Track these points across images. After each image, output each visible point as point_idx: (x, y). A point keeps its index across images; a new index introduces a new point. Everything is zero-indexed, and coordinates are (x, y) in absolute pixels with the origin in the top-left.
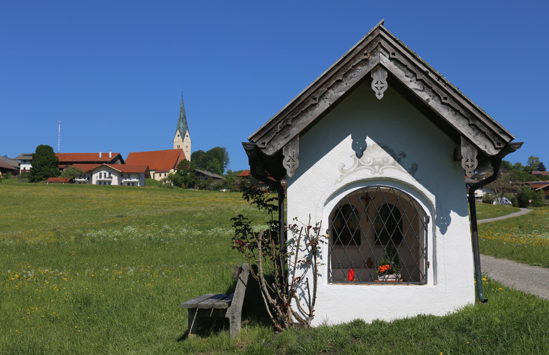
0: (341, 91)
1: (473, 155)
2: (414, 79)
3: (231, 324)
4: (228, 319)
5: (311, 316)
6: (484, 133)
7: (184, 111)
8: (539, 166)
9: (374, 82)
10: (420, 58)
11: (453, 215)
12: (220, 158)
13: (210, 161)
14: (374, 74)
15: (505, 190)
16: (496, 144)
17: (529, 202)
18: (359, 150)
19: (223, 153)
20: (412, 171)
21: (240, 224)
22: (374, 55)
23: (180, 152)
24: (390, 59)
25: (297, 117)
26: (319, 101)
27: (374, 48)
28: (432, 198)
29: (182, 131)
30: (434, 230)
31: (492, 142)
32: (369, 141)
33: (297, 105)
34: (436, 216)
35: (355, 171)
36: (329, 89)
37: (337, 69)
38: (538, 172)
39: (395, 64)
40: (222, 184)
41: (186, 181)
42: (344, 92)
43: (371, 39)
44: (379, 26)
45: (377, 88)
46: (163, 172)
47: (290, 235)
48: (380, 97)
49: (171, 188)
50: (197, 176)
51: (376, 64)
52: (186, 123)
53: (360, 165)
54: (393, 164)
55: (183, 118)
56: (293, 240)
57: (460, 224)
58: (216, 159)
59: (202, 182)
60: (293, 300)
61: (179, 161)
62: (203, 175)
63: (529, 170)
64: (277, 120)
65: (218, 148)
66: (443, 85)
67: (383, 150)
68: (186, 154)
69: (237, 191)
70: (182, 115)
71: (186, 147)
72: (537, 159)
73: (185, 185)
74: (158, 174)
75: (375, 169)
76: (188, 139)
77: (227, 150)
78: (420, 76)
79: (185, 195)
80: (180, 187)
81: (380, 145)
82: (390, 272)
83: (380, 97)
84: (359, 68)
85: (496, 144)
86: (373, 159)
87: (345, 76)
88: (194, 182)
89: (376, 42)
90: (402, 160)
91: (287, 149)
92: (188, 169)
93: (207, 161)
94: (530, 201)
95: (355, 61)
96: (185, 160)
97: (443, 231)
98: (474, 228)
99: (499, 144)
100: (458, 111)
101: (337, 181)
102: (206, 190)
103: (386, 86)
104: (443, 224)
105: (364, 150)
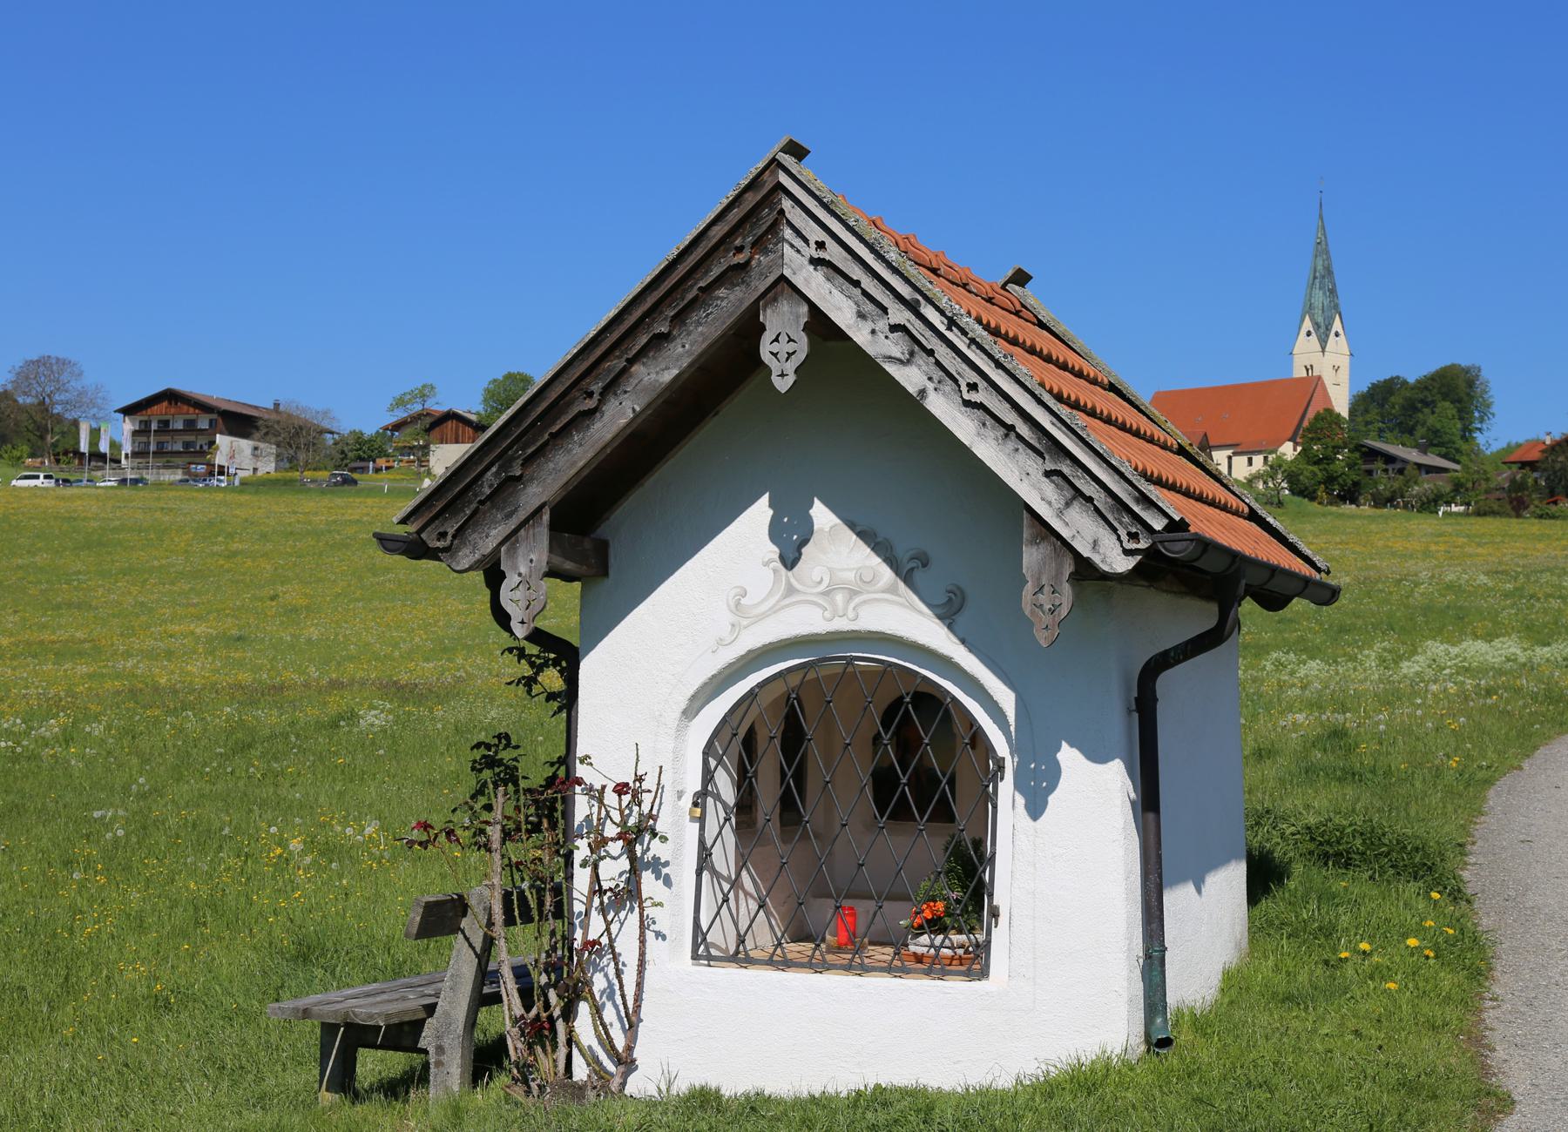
0: (667, 368)
1: (1058, 574)
5: (627, 1062)
6: (1090, 500)
7: (1327, 253)
9: (767, 337)
11: (1068, 756)
12: (1460, 401)
13: (1427, 411)
14: (769, 311)
16: (1124, 538)
18: (791, 543)
19: (1471, 384)
20: (949, 612)
21: (491, 762)
22: (766, 252)
23: (1313, 384)
25: (540, 452)
26: (601, 402)
27: (764, 228)
29: (1320, 319)
31: (1115, 530)
32: (821, 514)
33: (534, 415)
35: (774, 610)
36: (631, 362)
37: (650, 301)
40: (1447, 488)
41: (1330, 480)
42: (675, 372)
43: (751, 199)
44: (774, 160)
45: (775, 355)
46: (1259, 452)
47: (582, 808)
48: (783, 385)
49: (1280, 504)
50: (1365, 462)
51: (771, 279)
52: (1333, 292)
53: (791, 590)
54: (891, 590)
55: (1324, 277)
57: (1096, 790)
58: (1447, 404)
59: (1384, 482)
60: (584, 1008)
61: (1310, 415)
62: (1390, 459)
64: (477, 464)
65: (1453, 367)
67: (861, 543)
68: (1332, 391)
69: (1494, 513)
70: (1320, 267)
71: (1336, 372)
73: (1329, 492)
74: (1245, 459)
75: (833, 603)
76: (1339, 346)
77: (1485, 374)
78: (899, 315)
79: (1308, 527)
80: (1312, 498)
81: (852, 526)
83: (783, 385)
84: (722, 292)
86: (831, 570)
87: (680, 319)
88: (1356, 484)
89: (772, 210)
90: (918, 576)
91: (513, 551)
92: (1338, 440)
93: (1416, 410)
95: (707, 272)
96: (1330, 411)
97: (1036, 808)
98: (1148, 801)
99: (1133, 536)
101: (720, 642)
102: (1396, 507)
103: (802, 346)
105: (805, 542)
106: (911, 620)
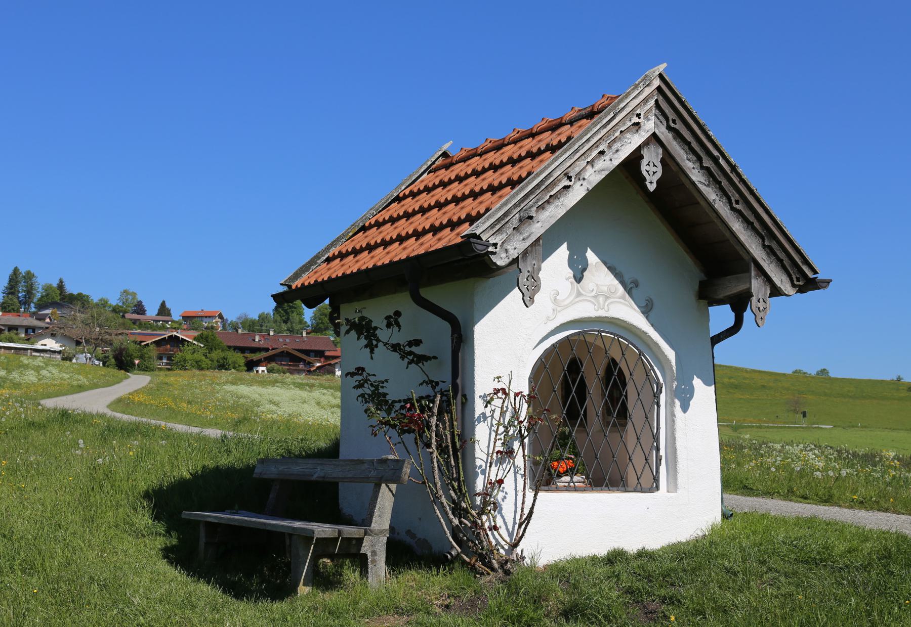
1: (765, 293)
2: (697, 165)
3: (370, 566)
4: (365, 556)
8: (135, 306)
9: (644, 162)
10: (711, 133)
15: (99, 342)
16: (795, 279)
17: (134, 364)
20: (647, 310)
24: (669, 128)
28: (671, 354)
30: (670, 405)
34: (675, 384)
35: (572, 303)
38: (135, 316)
39: (674, 138)
53: (579, 294)
54: (623, 298)
56: (484, 414)
63: (120, 311)
66: (736, 180)
72: (135, 294)
78: (707, 163)
81: (605, 263)
82: (570, 472)
85: (795, 279)
86: (597, 285)
90: (634, 291)
94: (137, 362)
97: (685, 408)
99: (798, 280)
100: (752, 223)
101: (548, 318)
104: (685, 397)
105: (584, 269)
106: (629, 312)
